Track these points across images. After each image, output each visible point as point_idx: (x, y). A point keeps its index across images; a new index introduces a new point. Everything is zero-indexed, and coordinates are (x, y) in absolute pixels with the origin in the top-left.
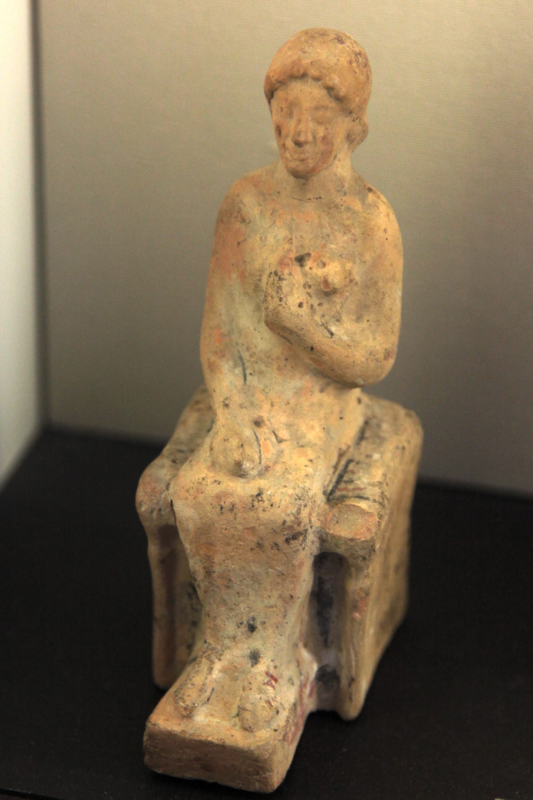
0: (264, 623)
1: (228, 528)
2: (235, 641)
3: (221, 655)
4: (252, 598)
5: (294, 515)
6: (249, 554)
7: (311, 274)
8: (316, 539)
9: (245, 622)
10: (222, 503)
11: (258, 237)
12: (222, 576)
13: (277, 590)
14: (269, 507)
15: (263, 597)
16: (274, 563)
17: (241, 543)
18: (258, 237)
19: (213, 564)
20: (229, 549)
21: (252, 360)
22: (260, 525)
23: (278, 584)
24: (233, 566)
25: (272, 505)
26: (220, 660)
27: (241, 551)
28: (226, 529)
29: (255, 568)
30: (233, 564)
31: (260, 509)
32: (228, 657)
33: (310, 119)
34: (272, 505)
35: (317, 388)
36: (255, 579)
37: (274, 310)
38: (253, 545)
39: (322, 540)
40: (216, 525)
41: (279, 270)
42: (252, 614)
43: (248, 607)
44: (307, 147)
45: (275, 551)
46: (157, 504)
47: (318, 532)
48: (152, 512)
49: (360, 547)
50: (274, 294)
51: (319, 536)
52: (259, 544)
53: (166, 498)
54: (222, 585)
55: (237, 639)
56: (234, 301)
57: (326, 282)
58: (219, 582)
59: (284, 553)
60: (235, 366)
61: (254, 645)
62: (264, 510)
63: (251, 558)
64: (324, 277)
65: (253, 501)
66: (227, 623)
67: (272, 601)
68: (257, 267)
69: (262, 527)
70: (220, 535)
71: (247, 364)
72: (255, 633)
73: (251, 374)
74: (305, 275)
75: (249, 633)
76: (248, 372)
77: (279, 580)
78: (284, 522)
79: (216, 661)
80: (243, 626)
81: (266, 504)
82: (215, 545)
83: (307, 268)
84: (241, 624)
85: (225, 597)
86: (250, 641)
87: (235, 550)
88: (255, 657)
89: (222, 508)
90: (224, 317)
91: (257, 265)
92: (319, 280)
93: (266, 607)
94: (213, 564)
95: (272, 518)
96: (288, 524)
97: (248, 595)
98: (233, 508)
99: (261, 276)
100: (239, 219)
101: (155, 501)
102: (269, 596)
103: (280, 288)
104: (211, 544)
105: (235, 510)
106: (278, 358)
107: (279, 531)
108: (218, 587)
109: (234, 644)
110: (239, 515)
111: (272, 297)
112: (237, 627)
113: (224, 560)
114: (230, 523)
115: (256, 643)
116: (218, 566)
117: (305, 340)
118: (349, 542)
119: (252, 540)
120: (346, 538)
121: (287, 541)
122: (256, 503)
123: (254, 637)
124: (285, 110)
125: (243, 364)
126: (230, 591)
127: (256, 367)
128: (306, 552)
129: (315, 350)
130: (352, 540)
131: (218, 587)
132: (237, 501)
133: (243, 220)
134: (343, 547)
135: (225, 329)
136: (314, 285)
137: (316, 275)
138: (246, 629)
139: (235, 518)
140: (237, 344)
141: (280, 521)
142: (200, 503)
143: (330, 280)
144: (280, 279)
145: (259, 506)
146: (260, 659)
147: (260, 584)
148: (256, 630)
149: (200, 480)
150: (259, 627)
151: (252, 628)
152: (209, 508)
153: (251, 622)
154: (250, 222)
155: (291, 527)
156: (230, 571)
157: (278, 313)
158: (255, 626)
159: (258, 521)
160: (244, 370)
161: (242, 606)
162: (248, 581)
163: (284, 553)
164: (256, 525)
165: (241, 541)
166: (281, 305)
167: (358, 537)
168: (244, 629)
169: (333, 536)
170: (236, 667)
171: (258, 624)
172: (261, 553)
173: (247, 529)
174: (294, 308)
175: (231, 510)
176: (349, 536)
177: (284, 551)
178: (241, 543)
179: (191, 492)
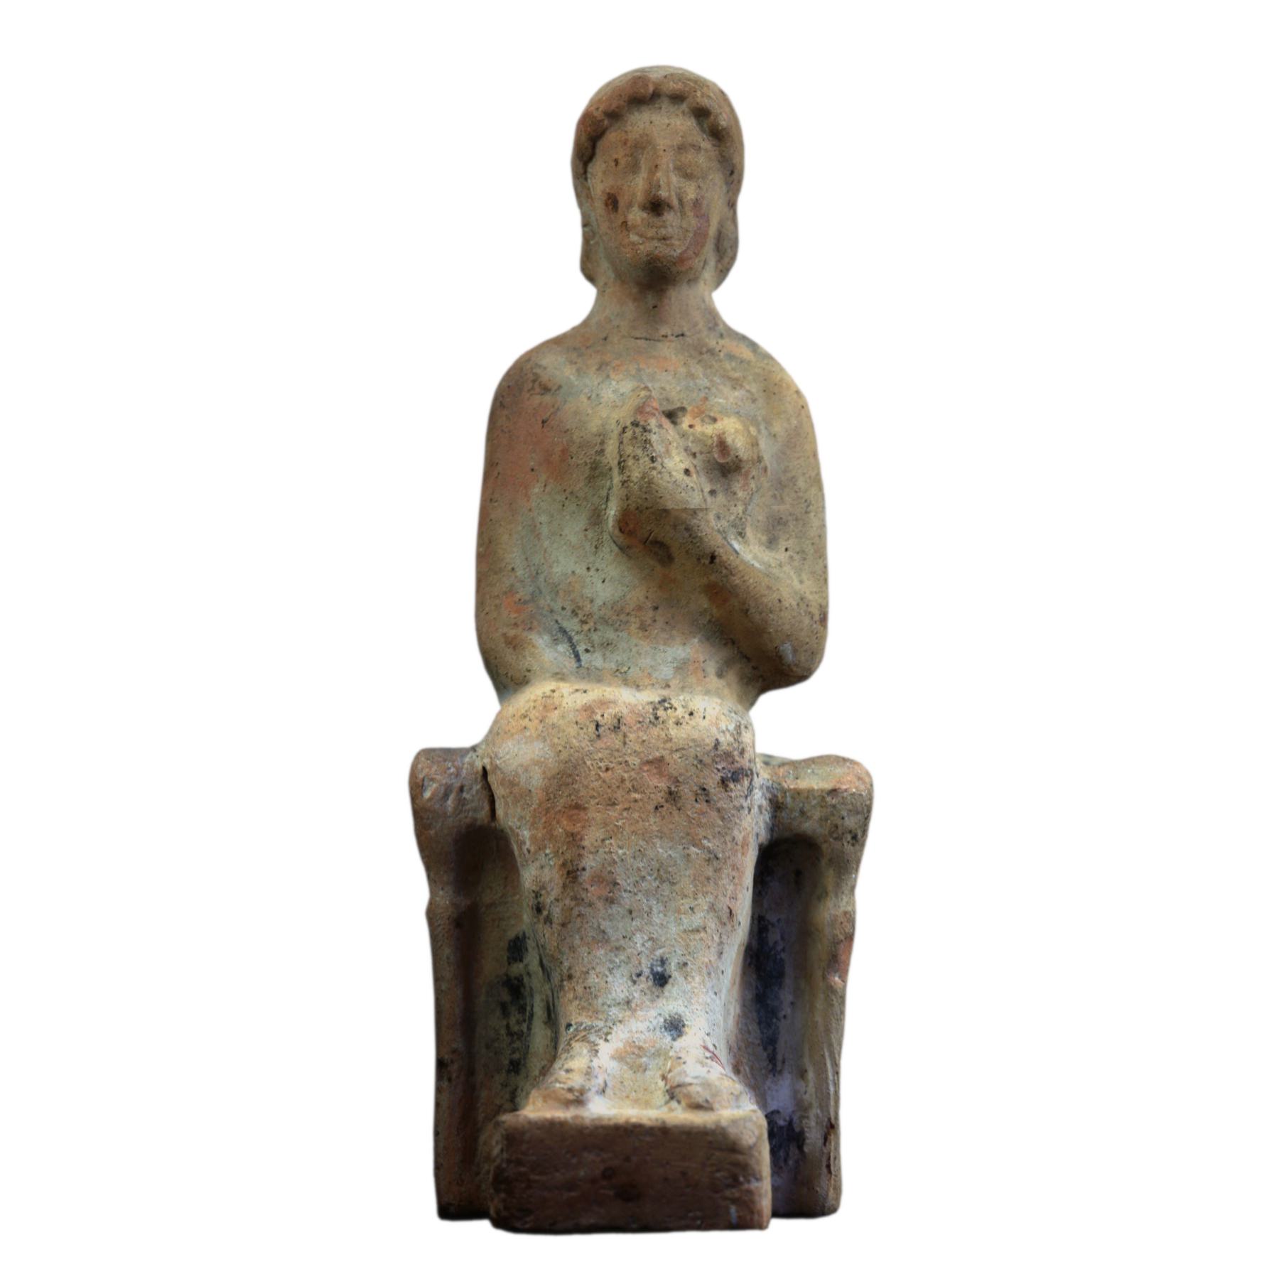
0: (685, 964)
1: (611, 765)
2: (630, 1009)
3: (607, 1034)
4: (657, 919)
5: (732, 735)
6: (652, 820)
7: (693, 435)
8: (765, 803)
9: (647, 972)
10: (598, 718)
11: (583, 398)
12: (598, 879)
13: (705, 894)
14: (687, 716)
15: (679, 912)
16: (701, 832)
17: (637, 796)
18: (583, 398)
19: (582, 852)
20: (613, 813)
21: (586, 627)
22: (672, 752)
23: (708, 879)
24: (620, 852)
25: (691, 714)
26: (606, 1040)
27: (636, 815)
28: (607, 769)
29: (662, 850)
30: (621, 848)
31: (671, 722)
32: (622, 1036)
33: (671, 165)
34: (691, 714)
35: (711, 668)
36: (664, 875)
37: (643, 478)
38: (659, 798)
39: (777, 805)
40: (589, 763)
41: (639, 418)
42: (659, 952)
43: (651, 939)
44: (669, 217)
45: (702, 806)
46: (457, 775)
47: (768, 788)
48: (446, 796)
49: (850, 807)
50: (639, 452)
51: (769, 795)
52: (670, 793)
53: (472, 764)
54: (599, 898)
55: (633, 1005)
56: (538, 536)
57: (723, 446)
58: (593, 893)
59: (719, 810)
60: (556, 641)
61: (671, 1007)
62: (678, 723)
63: (655, 828)
64: (719, 436)
65: (655, 709)
66: (610, 979)
67: (697, 920)
68: (594, 430)
69: (676, 756)
70: (596, 784)
71: (576, 638)
72: (668, 987)
73: (587, 651)
74: (683, 435)
75: (656, 990)
76: (581, 648)
77: (709, 872)
78: (717, 744)
79: (601, 1042)
80: (643, 978)
81: (680, 712)
82: (585, 809)
83: (685, 426)
84: (639, 975)
85: (605, 925)
86: (661, 1002)
87: (625, 814)
88: (675, 1026)
89: (598, 726)
90: (519, 573)
91: (594, 426)
92: (710, 442)
93: (685, 931)
94: (582, 852)
95: (696, 735)
96: (724, 747)
97: (649, 913)
98: (618, 725)
99: (602, 443)
100: (538, 390)
101: (452, 770)
102: (692, 909)
103: (647, 441)
104: (578, 807)
105: (623, 728)
106: (640, 608)
107: (707, 760)
108: (590, 905)
109: (628, 1013)
110: (632, 736)
111: (636, 458)
112: (630, 983)
113: (603, 840)
114: (616, 754)
115: (672, 1003)
116: (591, 856)
117: (701, 538)
118: (828, 799)
119: (658, 783)
120: (822, 791)
121: (724, 782)
122: (661, 713)
123: (666, 994)
124: (622, 162)
125: (570, 639)
126: (615, 909)
127: (595, 637)
128: (752, 826)
129: (717, 560)
130: (834, 792)
131: (590, 905)
132: (625, 711)
133: (546, 389)
134: (817, 814)
135: (523, 593)
136: (701, 453)
137: (703, 434)
138: (650, 983)
139: (625, 743)
140: (552, 611)
141: (710, 742)
142: (553, 726)
143: (729, 440)
144: (645, 430)
145: (669, 717)
146: (686, 1029)
147: (673, 884)
148: (671, 981)
149: (548, 693)
150: (675, 974)
151: (661, 980)
152: (573, 730)
153: (659, 969)
154: (560, 387)
155: (728, 755)
156: (615, 862)
157: (650, 482)
158: (667, 973)
159: (668, 745)
160: (573, 646)
161: (638, 938)
162: (650, 883)
163: (719, 810)
164: (665, 753)
165: (636, 790)
166: (654, 468)
167: (844, 787)
168: (645, 984)
169: (797, 793)
170: (640, 1048)
171: (672, 968)
172: (675, 813)
173: (649, 762)
174: (680, 476)
175: (616, 728)
176: (828, 786)
177: (719, 805)
178: (637, 796)
179: (533, 714)
